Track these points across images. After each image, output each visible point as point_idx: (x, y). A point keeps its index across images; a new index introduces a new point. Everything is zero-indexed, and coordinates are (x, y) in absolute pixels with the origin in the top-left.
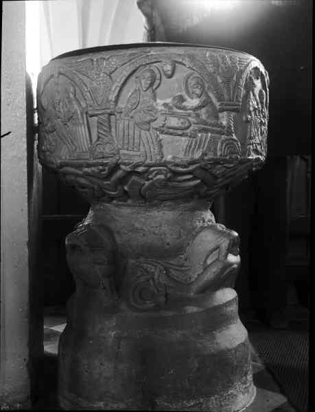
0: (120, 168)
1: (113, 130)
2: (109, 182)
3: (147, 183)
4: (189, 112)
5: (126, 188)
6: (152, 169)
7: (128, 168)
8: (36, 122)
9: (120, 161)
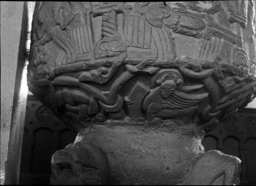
0: (125, 69)
1: (120, 28)
2: (108, 92)
3: (153, 91)
4: (203, 13)
5: (127, 99)
6: (162, 71)
7: (135, 69)
8: (28, 46)
9: (127, 59)
